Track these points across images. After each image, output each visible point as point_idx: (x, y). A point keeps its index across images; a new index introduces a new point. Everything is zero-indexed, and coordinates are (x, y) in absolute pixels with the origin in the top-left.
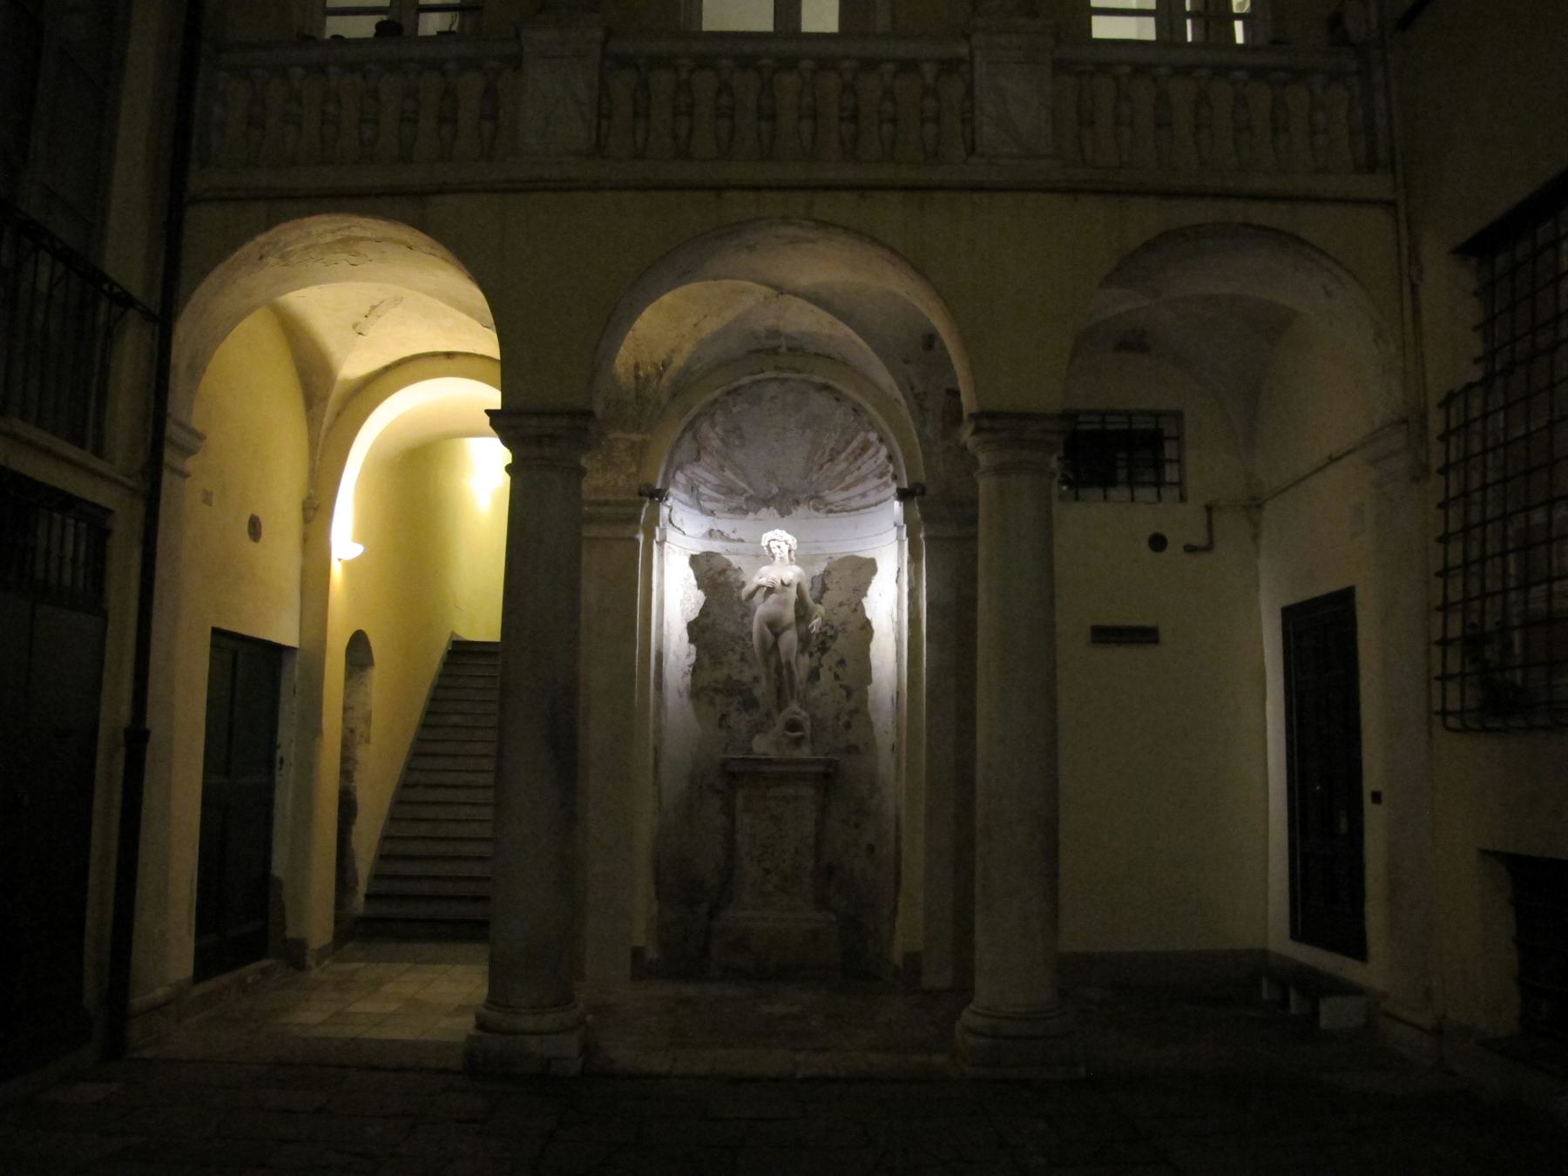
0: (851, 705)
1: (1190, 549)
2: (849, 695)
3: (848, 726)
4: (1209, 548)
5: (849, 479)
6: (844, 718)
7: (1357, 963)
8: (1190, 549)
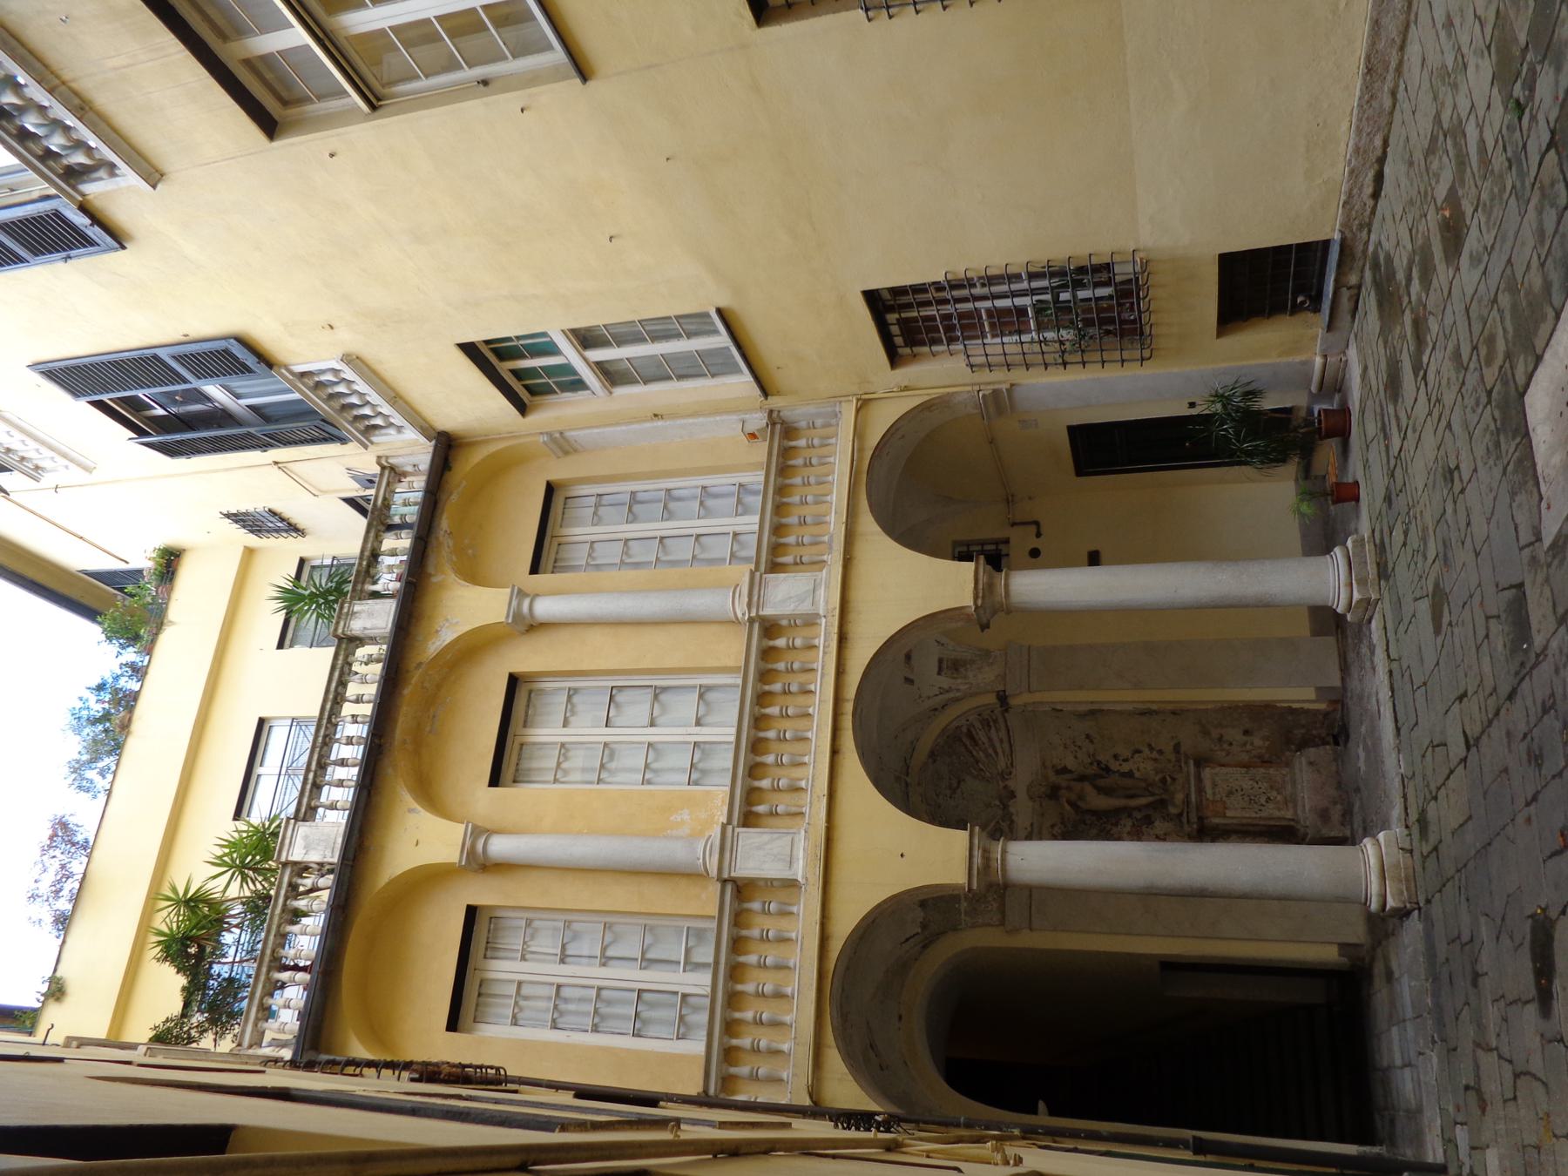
0: (1146, 751)
1: (1038, 535)
2: (1139, 751)
3: (1160, 752)
4: (1037, 523)
5: (990, 751)
6: (1155, 755)
7: (1075, 423)
8: (1038, 535)
